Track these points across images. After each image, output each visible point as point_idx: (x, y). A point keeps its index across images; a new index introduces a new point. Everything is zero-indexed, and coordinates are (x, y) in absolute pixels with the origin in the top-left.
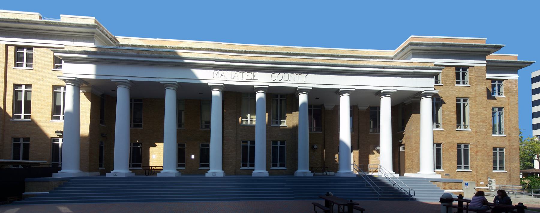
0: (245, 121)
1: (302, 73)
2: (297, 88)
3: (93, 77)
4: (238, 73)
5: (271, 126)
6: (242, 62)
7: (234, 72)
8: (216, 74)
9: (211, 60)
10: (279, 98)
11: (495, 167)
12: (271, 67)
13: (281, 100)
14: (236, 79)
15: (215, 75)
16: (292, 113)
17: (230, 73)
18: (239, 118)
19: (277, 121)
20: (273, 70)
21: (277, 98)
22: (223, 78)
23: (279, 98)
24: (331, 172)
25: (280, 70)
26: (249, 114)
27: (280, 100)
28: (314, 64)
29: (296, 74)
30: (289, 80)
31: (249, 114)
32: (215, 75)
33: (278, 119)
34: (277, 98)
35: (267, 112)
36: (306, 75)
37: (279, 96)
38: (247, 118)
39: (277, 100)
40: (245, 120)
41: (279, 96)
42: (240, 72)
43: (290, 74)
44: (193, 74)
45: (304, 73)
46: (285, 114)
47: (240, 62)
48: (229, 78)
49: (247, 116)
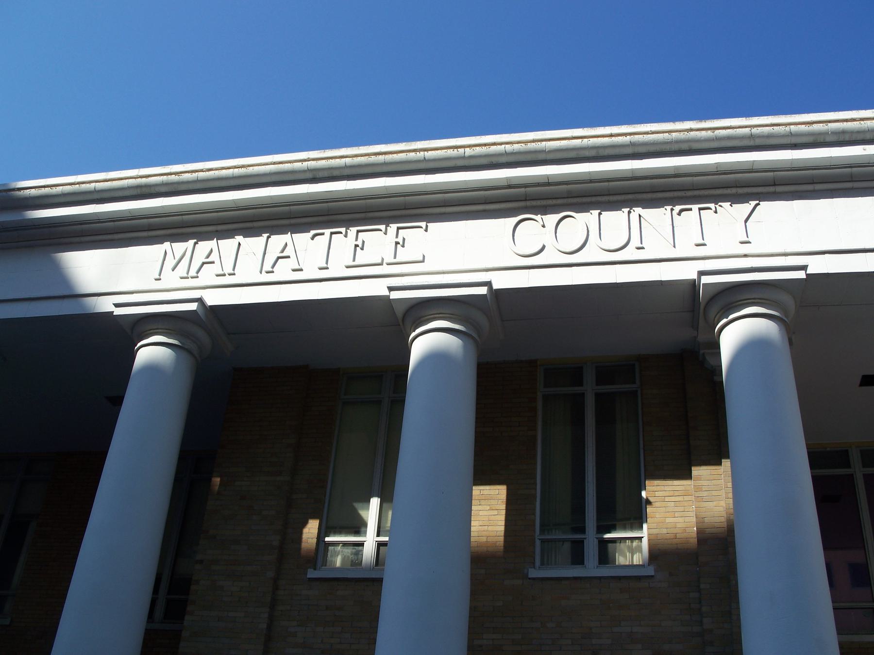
0: (348, 551)
1: (717, 199)
2: (693, 285)
3: (379, 499)
4: (302, 239)
5: (533, 573)
6: (326, 174)
7: (278, 241)
8: (178, 257)
9: (158, 189)
10: (590, 389)
11: (549, 541)
12: (510, 185)
13: (604, 403)
14: (283, 271)
15: (170, 262)
16: (688, 476)
17: (253, 245)
18: (305, 524)
19: (582, 542)
20: (526, 198)
21: (577, 389)
22: (208, 276)
23: (590, 389)
24: (610, 183)
25: (570, 195)
26: (375, 502)
27: (598, 396)
28: (794, 140)
29: (678, 208)
30: (635, 242)
31: (375, 502)
32: (170, 262)
33: (582, 530)
34: (577, 389)
35: (483, 477)
36: (747, 207)
37: (590, 377)
38: (359, 527)
39: (578, 402)
40: (345, 544)
41: (590, 377)
42: (313, 232)
43: (638, 210)
44: (60, 276)
45: (737, 199)
46: (641, 487)
47: (315, 176)
48: (248, 271)
49: (362, 513)
